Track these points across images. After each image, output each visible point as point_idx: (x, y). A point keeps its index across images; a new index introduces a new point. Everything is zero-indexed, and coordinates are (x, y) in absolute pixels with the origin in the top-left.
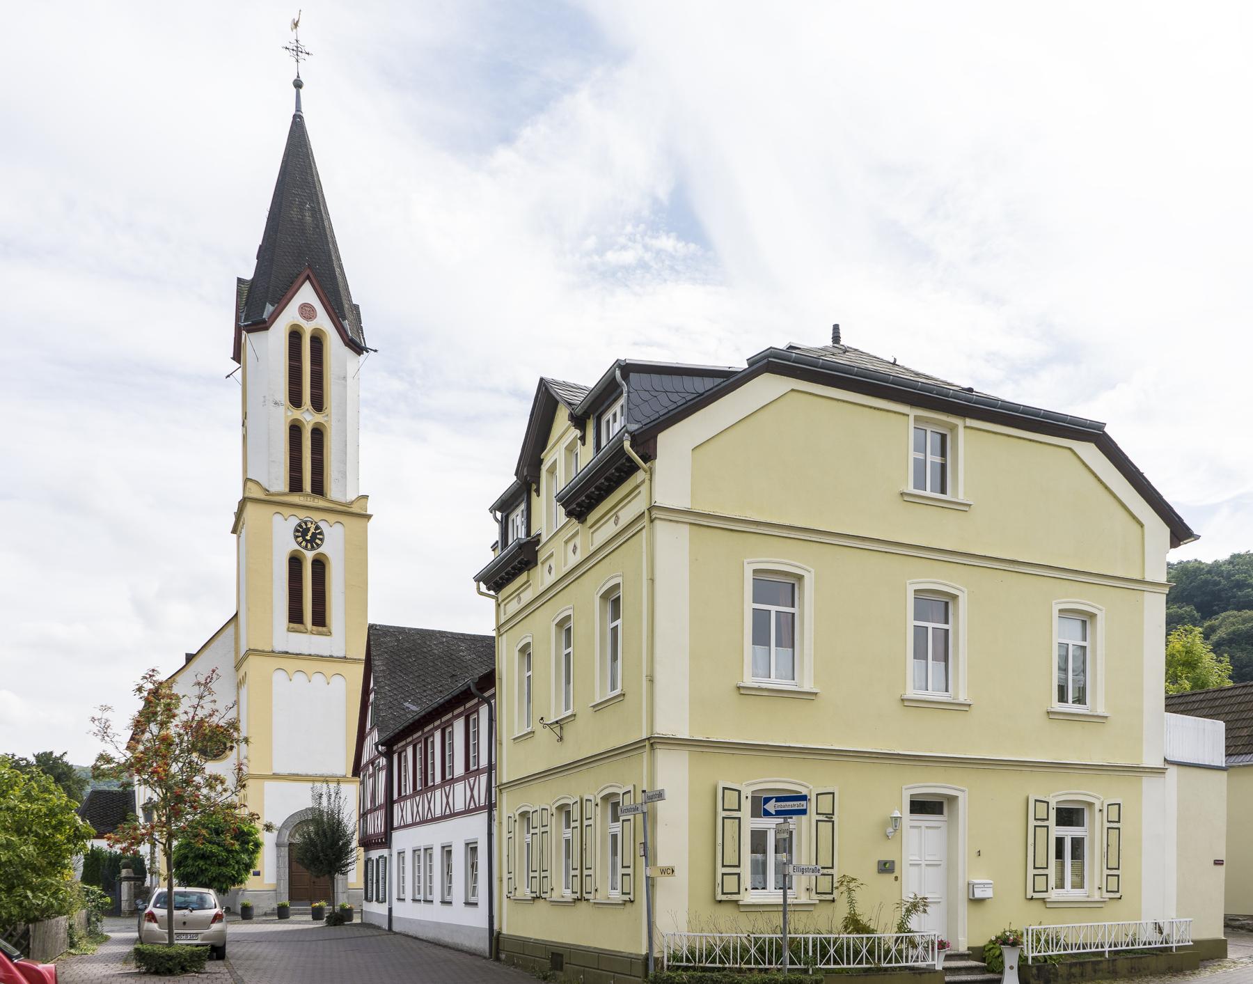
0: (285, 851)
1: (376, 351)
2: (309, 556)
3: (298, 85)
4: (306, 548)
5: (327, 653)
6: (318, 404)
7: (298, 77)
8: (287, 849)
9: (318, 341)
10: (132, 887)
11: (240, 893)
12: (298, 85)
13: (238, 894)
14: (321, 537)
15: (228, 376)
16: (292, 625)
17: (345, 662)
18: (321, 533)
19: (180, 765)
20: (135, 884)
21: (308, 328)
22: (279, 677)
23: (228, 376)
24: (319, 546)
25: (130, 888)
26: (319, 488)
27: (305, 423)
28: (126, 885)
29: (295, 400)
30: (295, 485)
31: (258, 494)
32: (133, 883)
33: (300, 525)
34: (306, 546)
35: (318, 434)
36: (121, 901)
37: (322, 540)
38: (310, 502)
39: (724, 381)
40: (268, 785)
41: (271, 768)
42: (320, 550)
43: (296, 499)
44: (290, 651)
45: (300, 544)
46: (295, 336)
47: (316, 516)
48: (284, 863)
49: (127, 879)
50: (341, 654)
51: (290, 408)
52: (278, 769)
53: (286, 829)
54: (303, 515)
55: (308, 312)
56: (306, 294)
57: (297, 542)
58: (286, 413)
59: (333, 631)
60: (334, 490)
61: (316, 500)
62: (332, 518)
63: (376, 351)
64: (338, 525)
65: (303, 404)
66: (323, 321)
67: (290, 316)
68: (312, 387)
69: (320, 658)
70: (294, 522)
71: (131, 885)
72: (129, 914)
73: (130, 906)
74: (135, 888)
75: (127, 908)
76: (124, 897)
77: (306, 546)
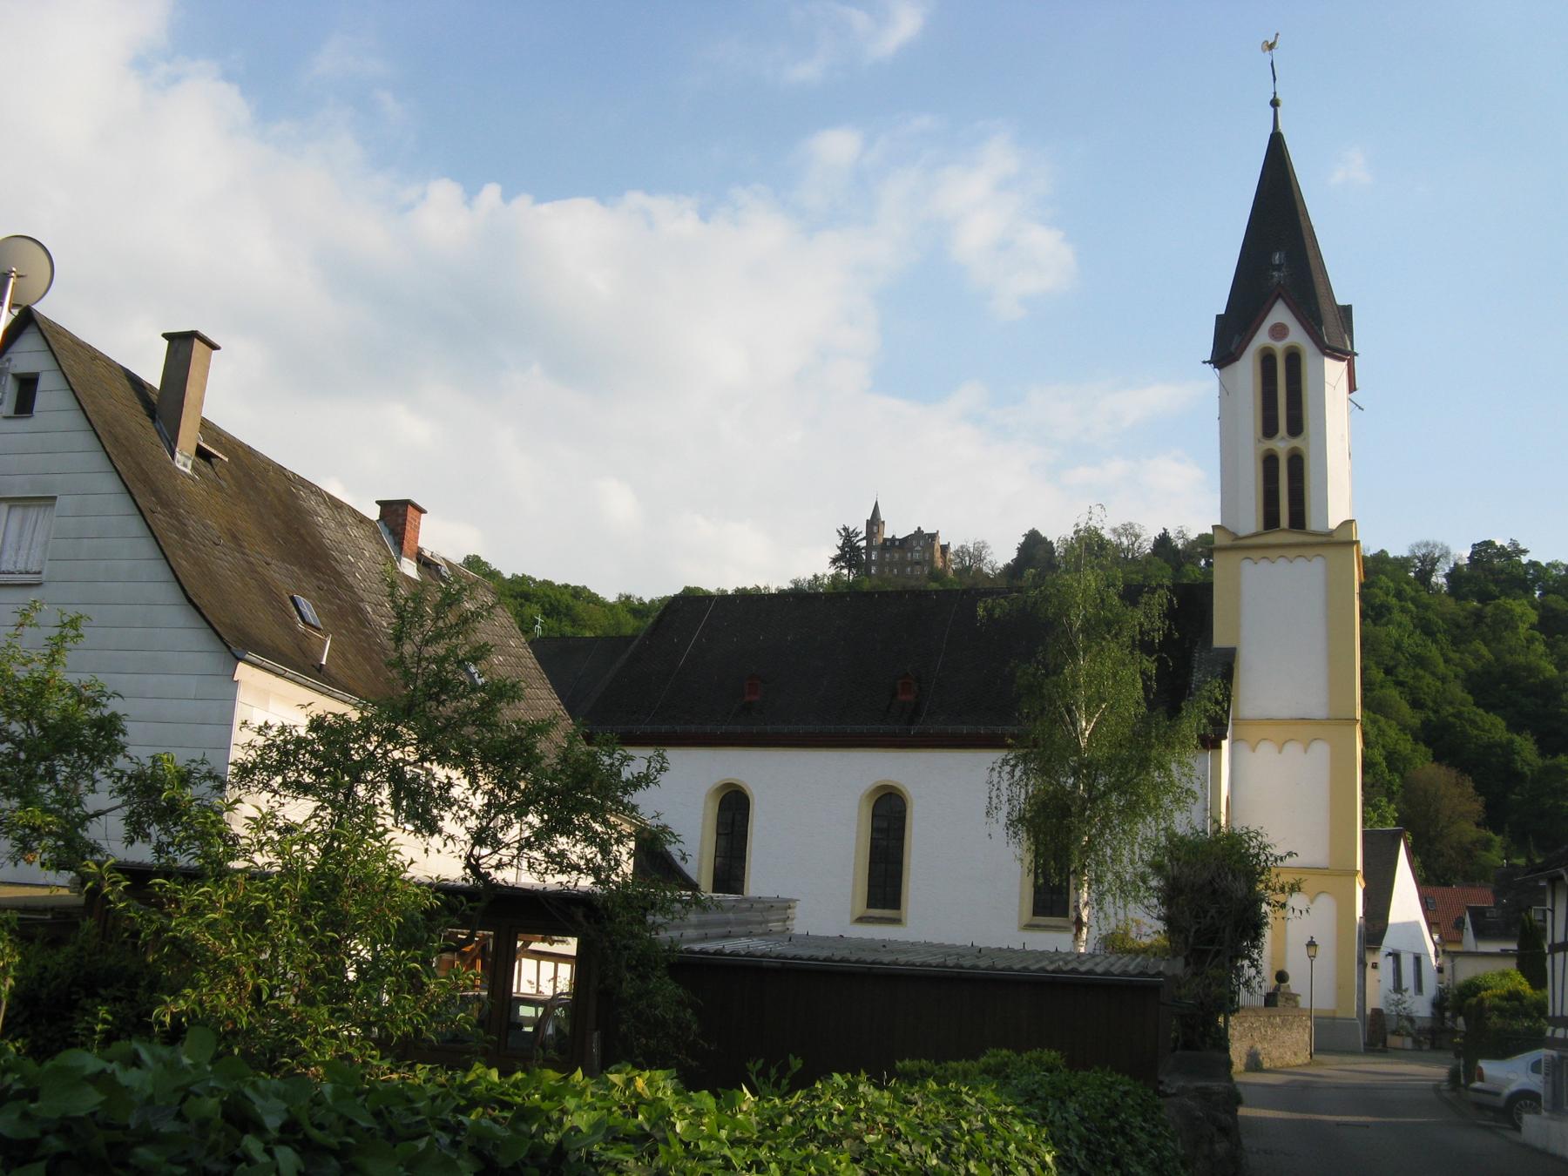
3: (1275, 103)
7: (1275, 93)
9: (1294, 358)
12: (1275, 103)
21: (1279, 347)
26: (1298, 520)
30: (1271, 521)
46: (1268, 359)
56: (1280, 314)
60: (1313, 524)
63: (1204, 362)
66: (1297, 336)
67: (1262, 339)
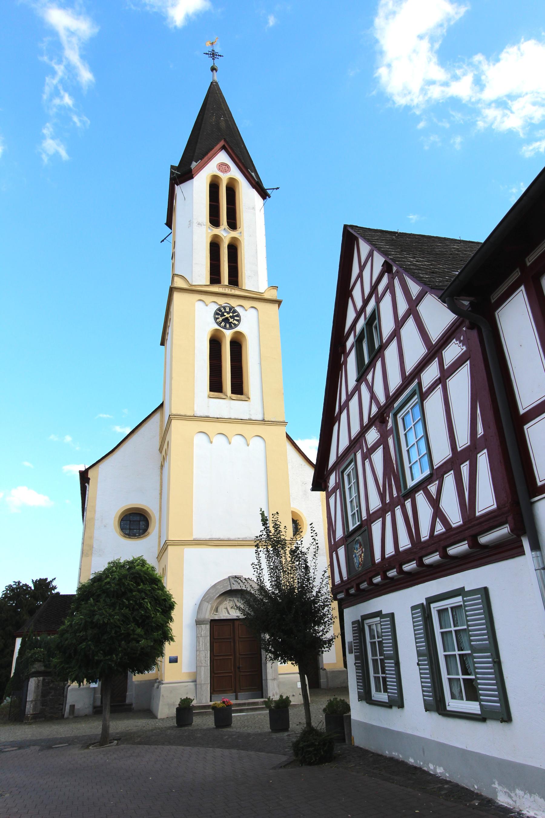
0: (206, 629)
1: (278, 188)
2: (228, 334)
4: (225, 327)
5: (246, 417)
6: (233, 224)
8: (208, 626)
10: (40, 684)
11: (156, 685)
13: (153, 686)
14: (238, 318)
15: (163, 241)
16: (212, 393)
17: (264, 424)
18: (238, 316)
19: (111, 619)
20: (44, 680)
21: (224, 178)
22: (200, 440)
23: (163, 241)
24: (236, 326)
25: (37, 686)
26: (234, 280)
27: (223, 238)
28: (33, 682)
29: (215, 221)
30: (215, 278)
31: (183, 285)
32: (41, 678)
33: (219, 310)
34: (225, 326)
35: (233, 249)
36: (26, 701)
37: (239, 321)
38: (228, 291)
39: (477, 552)
40: (189, 552)
41: (192, 534)
42: (237, 329)
43: (215, 289)
44: (210, 416)
45: (219, 324)
46: (214, 187)
47: (234, 303)
48: (206, 644)
49: (37, 674)
50: (260, 417)
51: (211, 227)
52: (198, 534)
53: (208, 602)
54: (222, 301)
55: (223, 167)
57: (217, 323)
58: (207, 231)
59: (251, 396)
61: (236, 291)
62: (247, 304)
64: (253, 310)
65: (221, 223)
66: (235, 173)
68: (229, 277)
69: (241, 421)
70: (215, 307)
71: (39, 681)
72: (32, 719)
73: (35, 708)
74: (43, 684)
75: (31, 712)
76: (30, 697)
77: (225, 326)
